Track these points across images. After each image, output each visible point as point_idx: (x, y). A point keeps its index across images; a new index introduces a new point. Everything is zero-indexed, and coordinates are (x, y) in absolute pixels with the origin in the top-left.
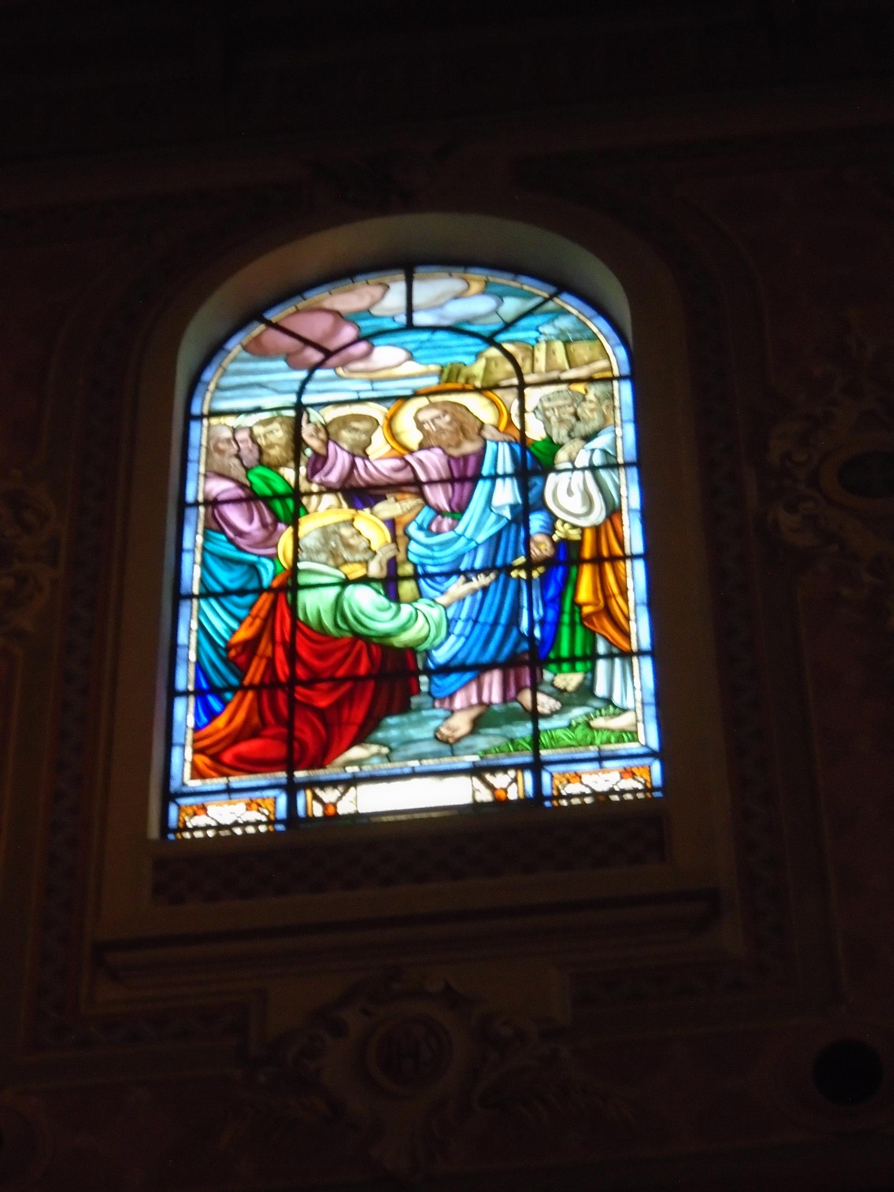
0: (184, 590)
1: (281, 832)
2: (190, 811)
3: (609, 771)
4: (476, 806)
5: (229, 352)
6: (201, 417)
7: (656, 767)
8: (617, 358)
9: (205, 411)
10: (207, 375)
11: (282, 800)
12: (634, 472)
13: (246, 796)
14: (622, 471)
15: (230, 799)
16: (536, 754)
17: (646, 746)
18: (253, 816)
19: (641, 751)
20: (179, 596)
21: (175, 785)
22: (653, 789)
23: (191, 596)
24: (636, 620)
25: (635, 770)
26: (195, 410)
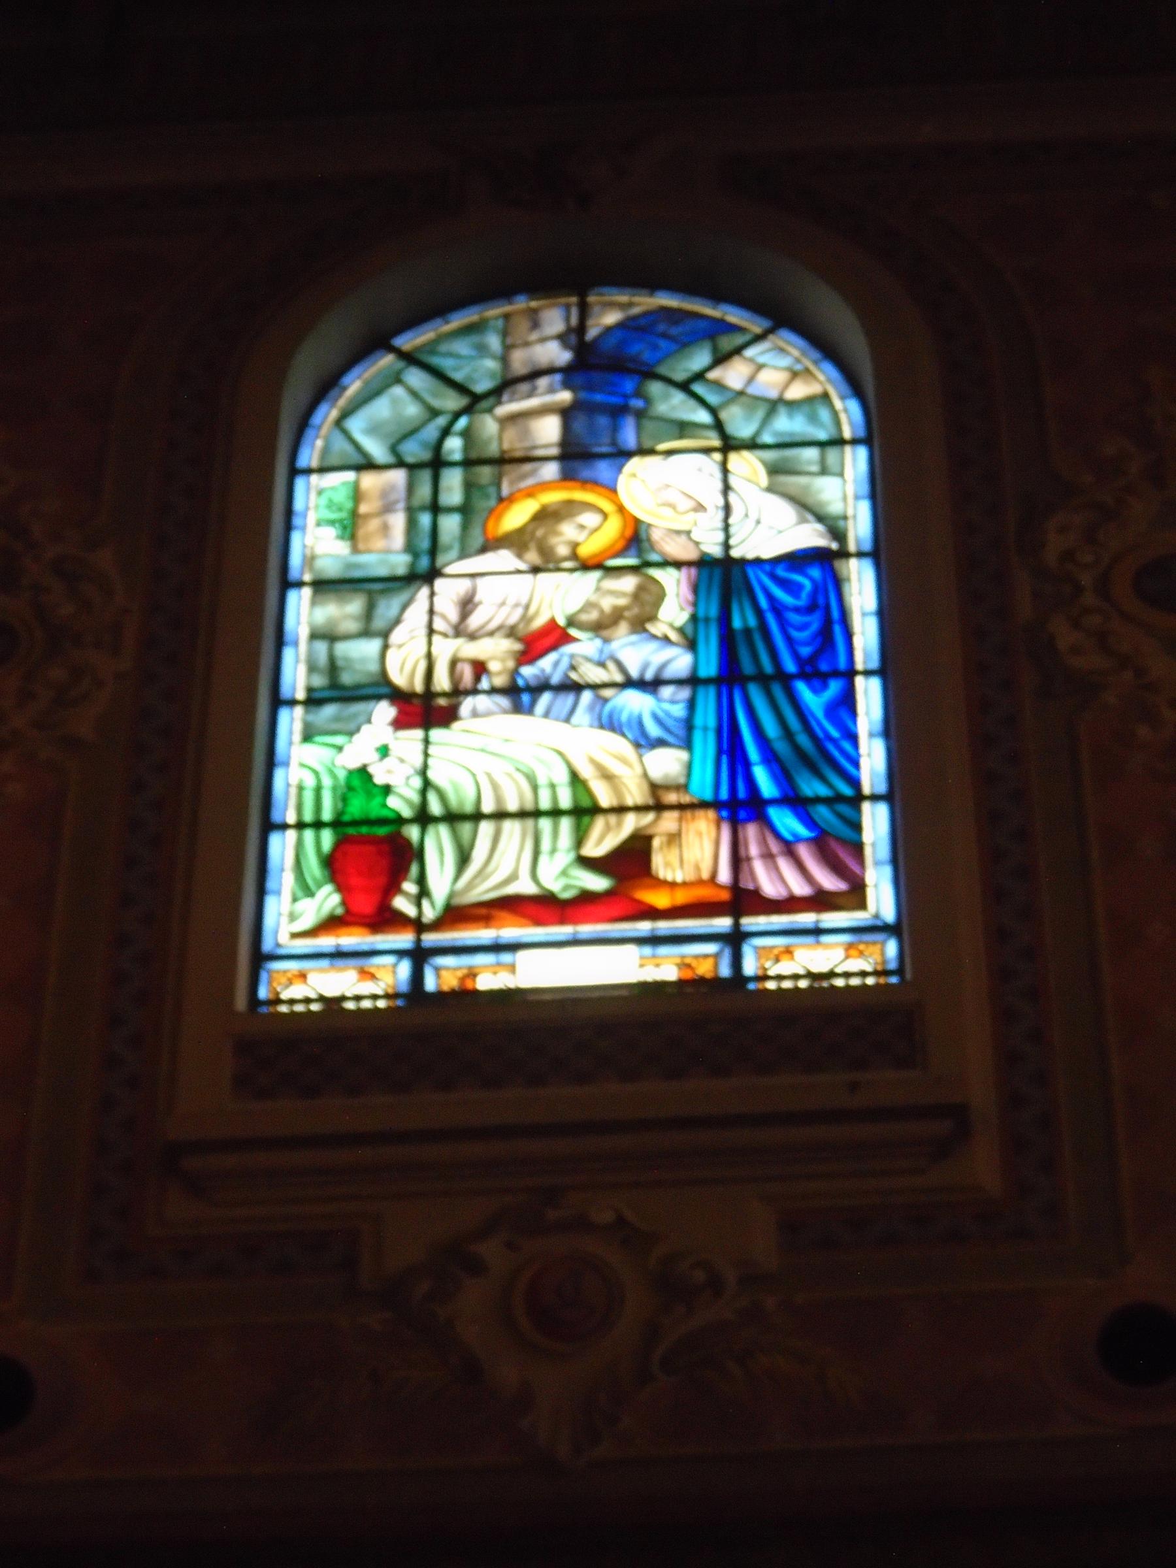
0: (276, 817)
1: (399, 1008)
2: (284, 980)
3: (828, 946)
5: (345, 389)
6: (309, 471)
7: (892, 948)
8: (850, 415)
11: (405, 968)
12: (862, 453)
14: (848, 449)
17: (877, 916)
20: (278, 702)
21: (267, 946)
22: (885, 973)
23: (293, 703)
24: (860, 580)
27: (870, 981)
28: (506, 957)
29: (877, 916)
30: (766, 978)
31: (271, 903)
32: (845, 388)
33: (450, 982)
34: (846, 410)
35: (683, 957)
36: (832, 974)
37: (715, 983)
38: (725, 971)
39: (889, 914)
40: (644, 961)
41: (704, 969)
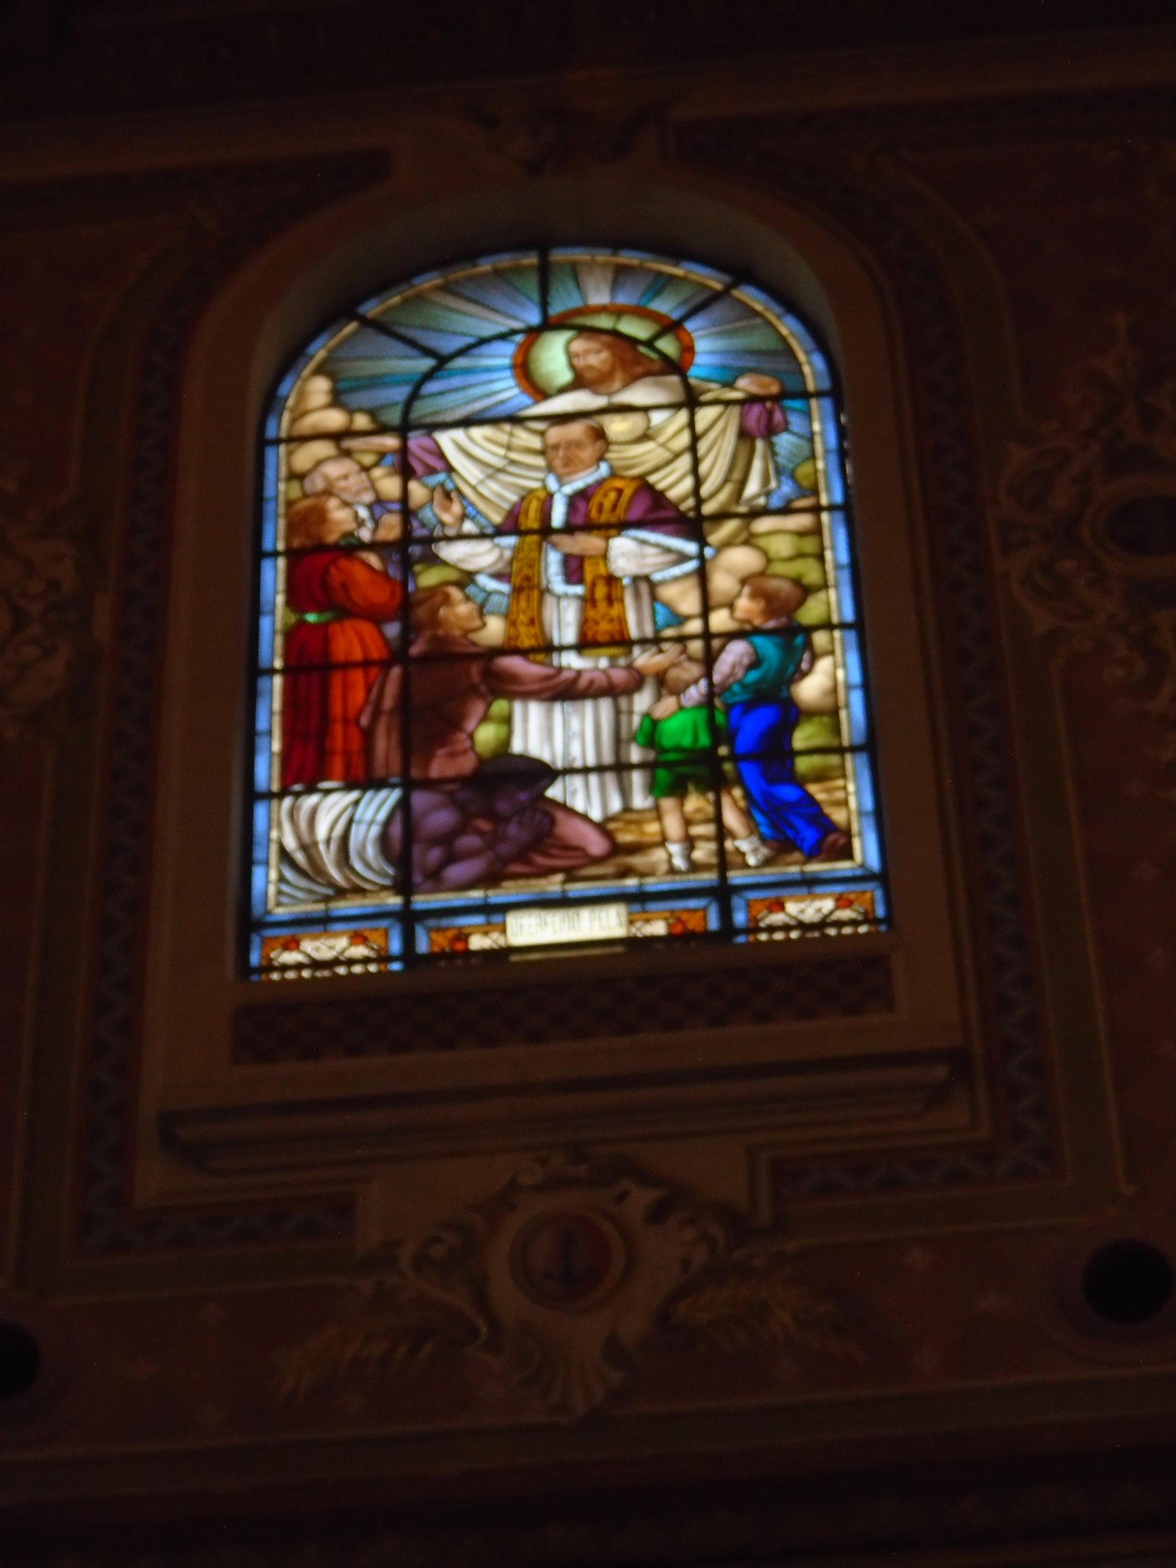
4: (631, 943)
5: (312, 357)
6: (277, 442)
9: (283, 434)
10: (283, 389)
13: (839, 889)
15: (325, 930)
16: (723, 877)
18: (360, 951)
19: (859, 872)
25: (366, 934)
26: (271, 433)
27: (372, 968)
28: (496, 918)
29: (862, 866)
30: (758, 930)
31: (258, 873)
32: (810, 343)
33: (442, 941)
34: (810, 363)
35: (672, 911)
36: (336, 962)
37: (706, 936)
38: (713, 924)
39: (874, 861)
40: (634, 917)
41: (694, 924)
